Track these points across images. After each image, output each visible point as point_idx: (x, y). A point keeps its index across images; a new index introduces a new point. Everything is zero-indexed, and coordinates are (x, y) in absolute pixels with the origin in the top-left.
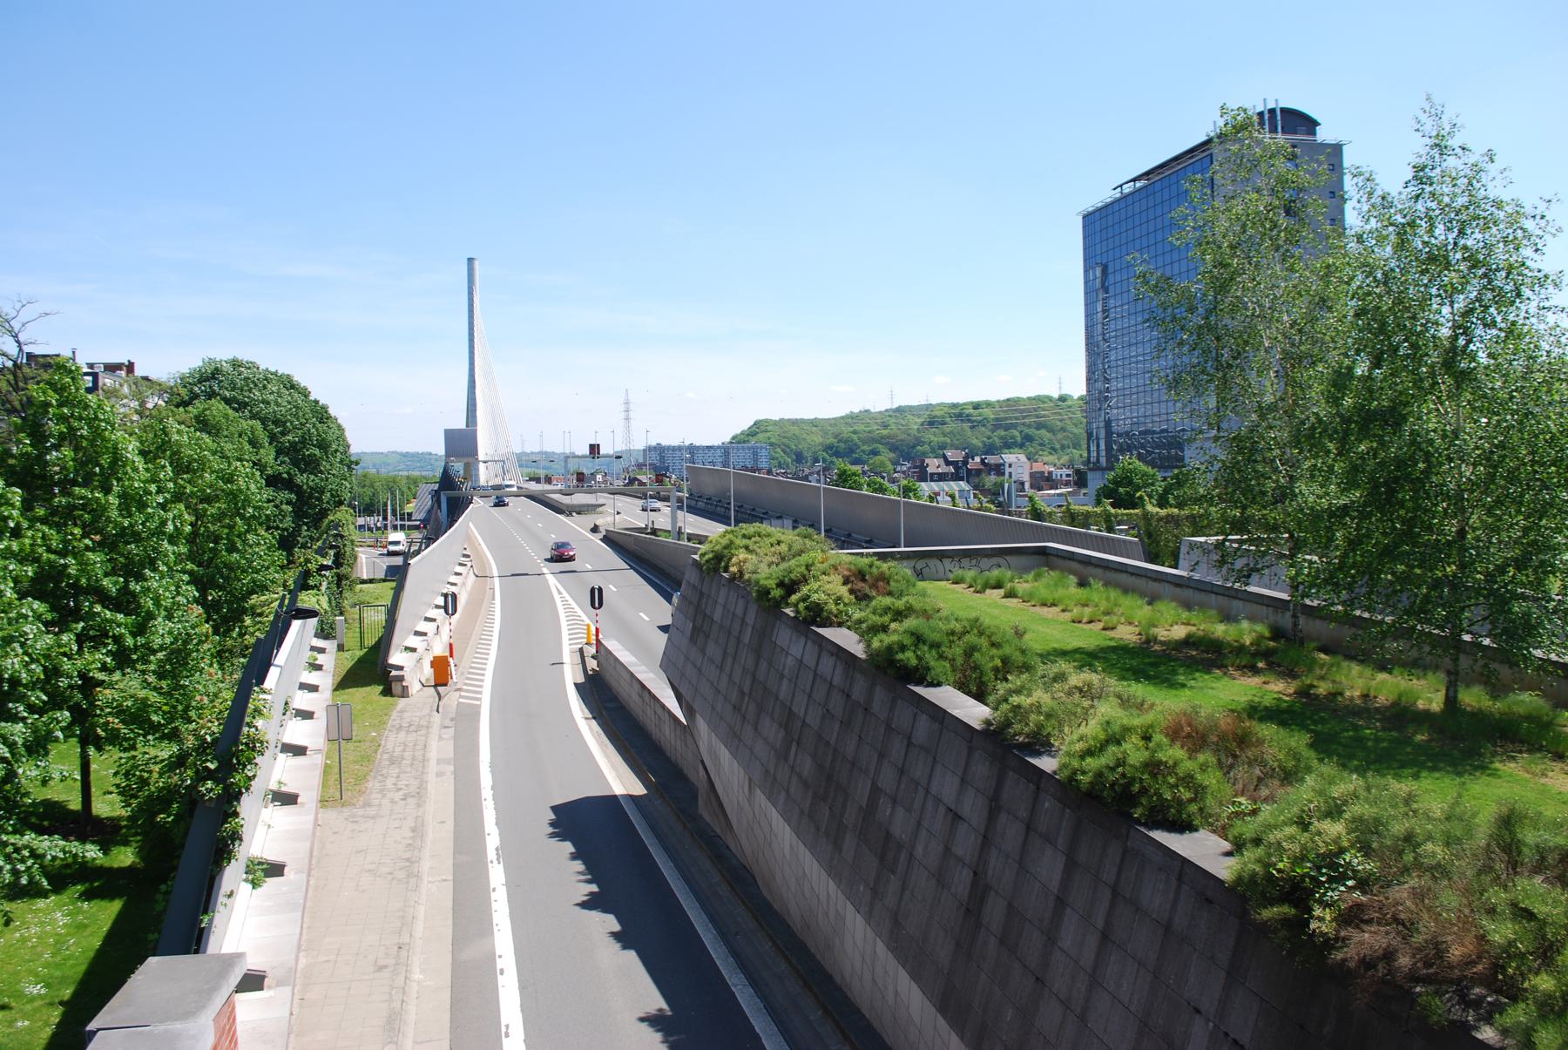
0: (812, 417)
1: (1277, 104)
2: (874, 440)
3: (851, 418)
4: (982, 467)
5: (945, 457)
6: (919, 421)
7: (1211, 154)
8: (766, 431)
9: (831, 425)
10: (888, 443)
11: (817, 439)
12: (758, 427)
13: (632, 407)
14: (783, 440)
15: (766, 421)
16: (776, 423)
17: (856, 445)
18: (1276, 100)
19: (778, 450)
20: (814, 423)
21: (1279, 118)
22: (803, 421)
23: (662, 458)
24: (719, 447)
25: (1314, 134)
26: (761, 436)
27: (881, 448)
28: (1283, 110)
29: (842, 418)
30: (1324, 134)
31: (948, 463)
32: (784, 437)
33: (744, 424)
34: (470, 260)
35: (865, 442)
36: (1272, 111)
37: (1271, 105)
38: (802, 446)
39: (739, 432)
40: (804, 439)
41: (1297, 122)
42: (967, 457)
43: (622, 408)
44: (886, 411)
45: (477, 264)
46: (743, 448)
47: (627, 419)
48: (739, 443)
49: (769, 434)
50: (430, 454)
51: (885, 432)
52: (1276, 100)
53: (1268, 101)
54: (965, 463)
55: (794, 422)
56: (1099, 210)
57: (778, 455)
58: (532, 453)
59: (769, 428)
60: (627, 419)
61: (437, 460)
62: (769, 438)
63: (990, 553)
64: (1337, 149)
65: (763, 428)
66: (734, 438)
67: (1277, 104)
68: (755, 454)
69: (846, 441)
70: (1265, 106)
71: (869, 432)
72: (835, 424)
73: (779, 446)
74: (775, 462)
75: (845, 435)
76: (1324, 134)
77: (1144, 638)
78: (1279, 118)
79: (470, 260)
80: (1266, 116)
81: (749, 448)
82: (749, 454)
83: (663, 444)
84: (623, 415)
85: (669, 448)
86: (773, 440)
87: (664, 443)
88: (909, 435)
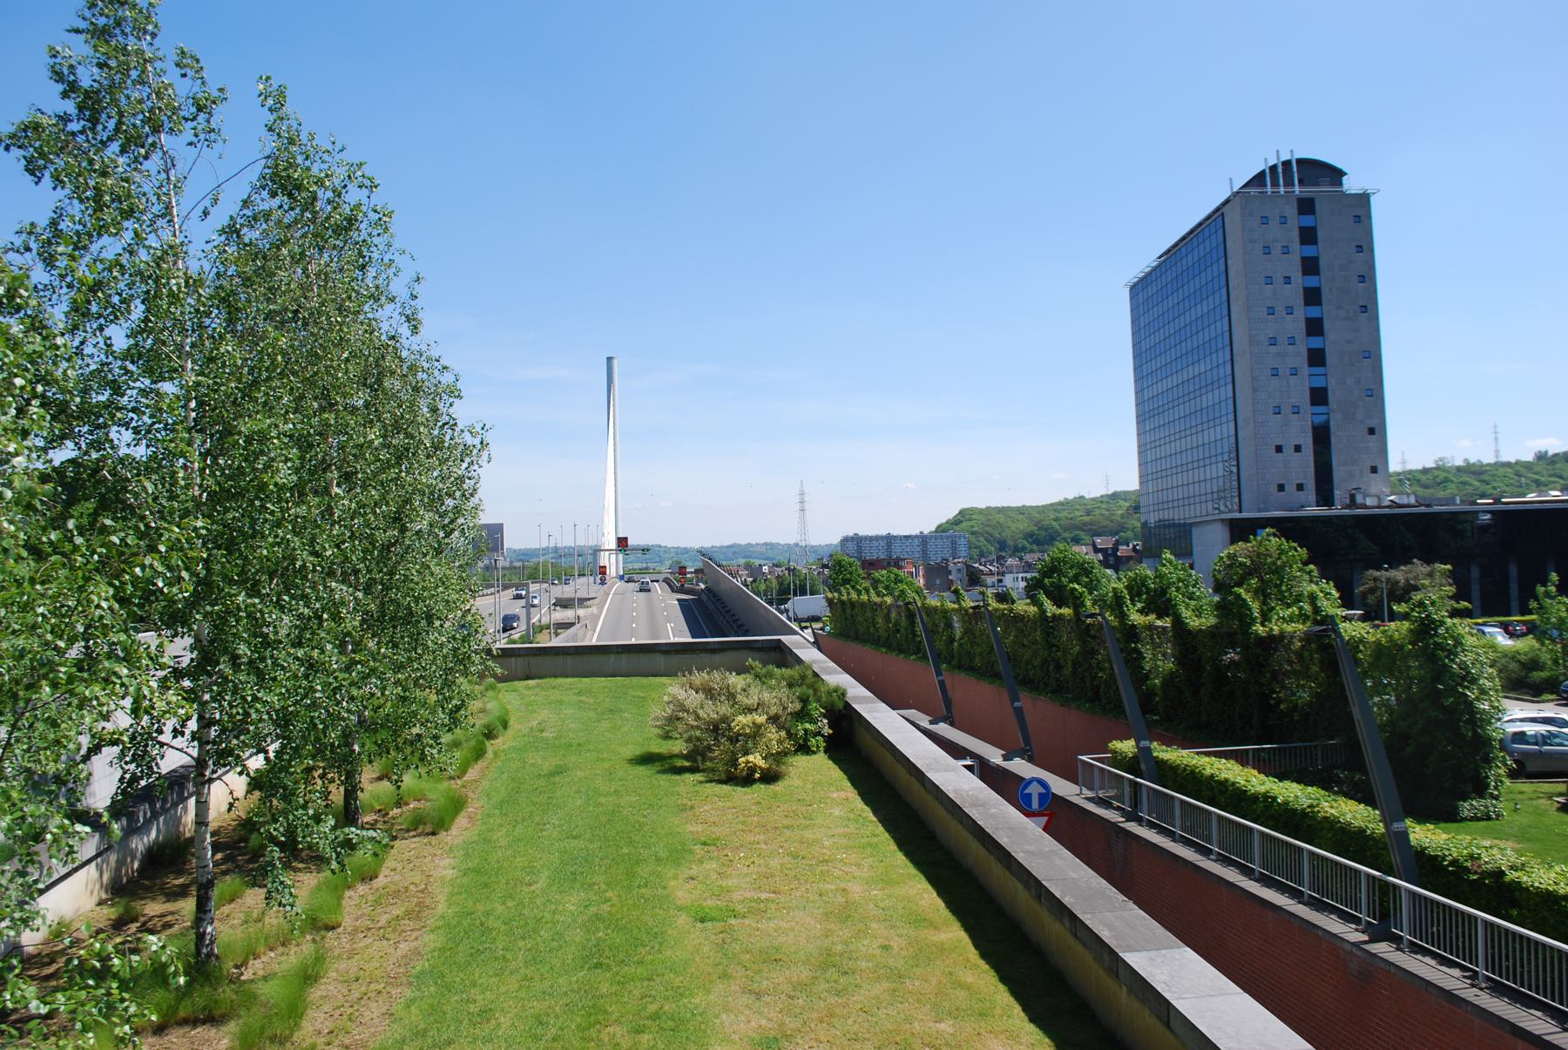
0: (1020, 505)
1: (1292, 156)
2: (1076, 527)
3: (1065, 504)
4: (1133, 554)
5: (1094, 545)
6: (1127, 504)
7: (1223, 214)
8: (970, 520)
9: (1039, 513)
10: (1090, 530)
11: (1024, 525)
12: (964, 515)
13: (807, 498)
14: (987, 529)
15: (971, 509)
16: (981, 511)
17: (1057, 532)
18: (1292, 151)
19: (982, 539)
20: (1022, 511)
21: (1295, 169)
22: (1009, 509)
23: (859, 549)
24: (916, 536)
25: (1340, 184)
26: (964, 524)
27: (1082, 535)
28: (1299, 161)
29: (1051, 505)
30: (1351, 185)
31: (1096, 550)
32: (989, 526)
33: (950, 513)
34: (610, 359)
35: (1065, 529)
36: (1287, 164)
37: (1285, 157)
38: (1007, 534)
39: (944, 521)
40: (1009, 527)
41: (1320, 173)
42: (1117, 543)
43: (797, 499)
44: (1102, 496)
45: (615, 362)
46: (942, 537)
47: (803, 510)
48: (943, 531)
49: (972, 523)
50: (660, 546)
51: (1087, 519)
52: (1292, 151)
53: (1281, 153)
54: (1115, 549)
55: (1001, 510)
56: (1141, 280)
57: (980, 544)
58: (757, 544)
59: (973, 517)
60: (803, 510)
61: (665, 552)
62: (972, 527)
63: (678, 648)
64: (1363, 199)
65: (968, 517)
66: (939, 527)
67: (1292, 156)
68: (954, 543)
69: (1047, 529)
70: (1278, 158)
71: (1071, 519)
72: (1043, 512)
73: (982, 535)
74: (975, 552)
75: (1046, 523)
76: (1351, 185)
77: (115, 761)
78: (1295, 169)
79: (610, 359)
80: (1280, 170)
81: (947, 538)
82: (947, 543)
83: (860, 534)
84: (798, 507)
85: (867, 538)
86: (976, 529)
87: (862, 533)
88: (1112, 521)
